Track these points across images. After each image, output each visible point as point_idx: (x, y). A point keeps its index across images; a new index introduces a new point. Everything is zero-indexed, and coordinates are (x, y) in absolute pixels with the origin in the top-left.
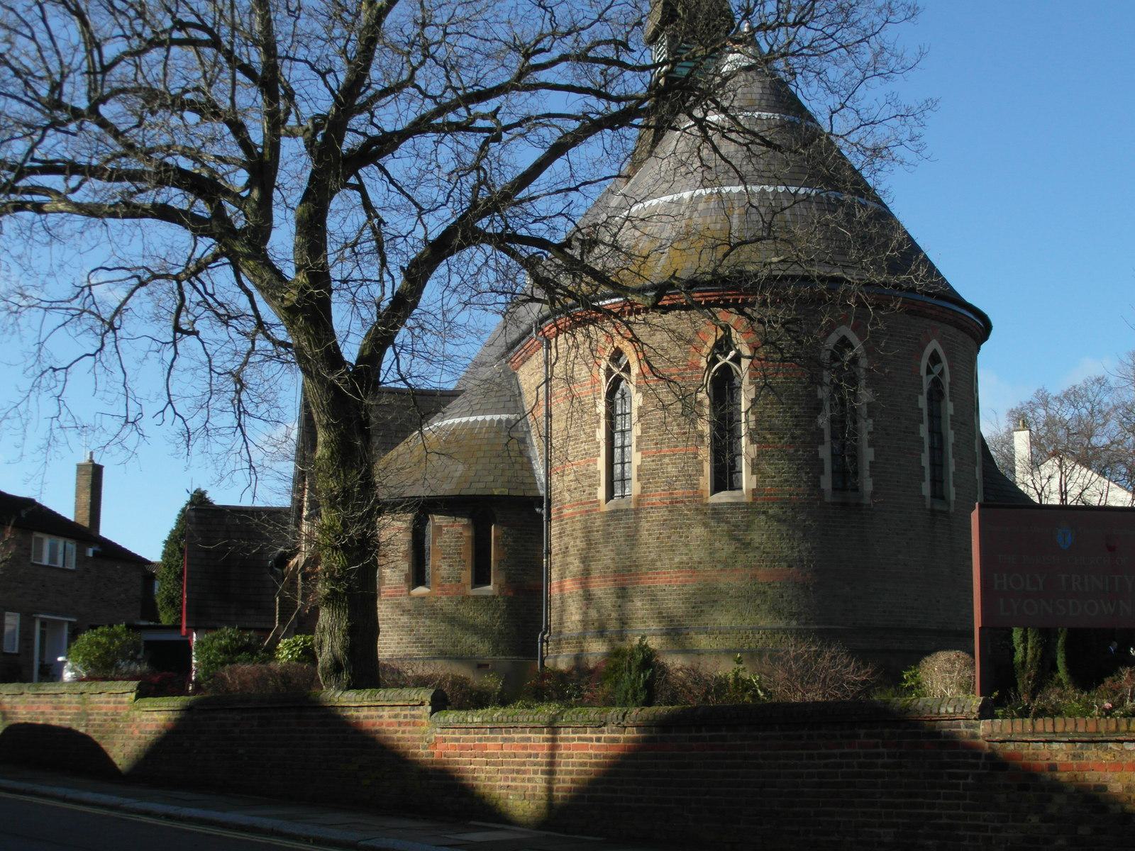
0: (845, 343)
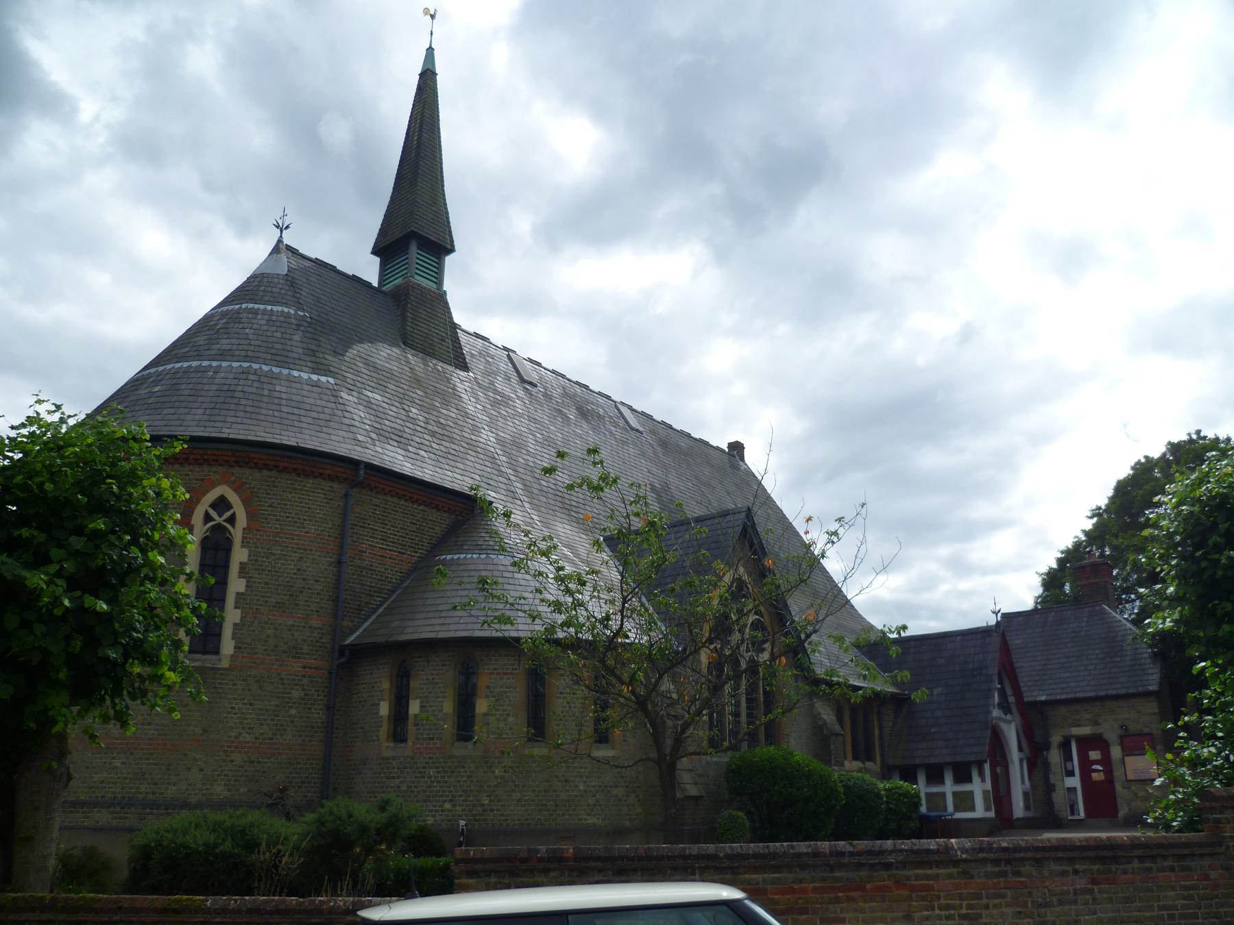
0: (221, 504)
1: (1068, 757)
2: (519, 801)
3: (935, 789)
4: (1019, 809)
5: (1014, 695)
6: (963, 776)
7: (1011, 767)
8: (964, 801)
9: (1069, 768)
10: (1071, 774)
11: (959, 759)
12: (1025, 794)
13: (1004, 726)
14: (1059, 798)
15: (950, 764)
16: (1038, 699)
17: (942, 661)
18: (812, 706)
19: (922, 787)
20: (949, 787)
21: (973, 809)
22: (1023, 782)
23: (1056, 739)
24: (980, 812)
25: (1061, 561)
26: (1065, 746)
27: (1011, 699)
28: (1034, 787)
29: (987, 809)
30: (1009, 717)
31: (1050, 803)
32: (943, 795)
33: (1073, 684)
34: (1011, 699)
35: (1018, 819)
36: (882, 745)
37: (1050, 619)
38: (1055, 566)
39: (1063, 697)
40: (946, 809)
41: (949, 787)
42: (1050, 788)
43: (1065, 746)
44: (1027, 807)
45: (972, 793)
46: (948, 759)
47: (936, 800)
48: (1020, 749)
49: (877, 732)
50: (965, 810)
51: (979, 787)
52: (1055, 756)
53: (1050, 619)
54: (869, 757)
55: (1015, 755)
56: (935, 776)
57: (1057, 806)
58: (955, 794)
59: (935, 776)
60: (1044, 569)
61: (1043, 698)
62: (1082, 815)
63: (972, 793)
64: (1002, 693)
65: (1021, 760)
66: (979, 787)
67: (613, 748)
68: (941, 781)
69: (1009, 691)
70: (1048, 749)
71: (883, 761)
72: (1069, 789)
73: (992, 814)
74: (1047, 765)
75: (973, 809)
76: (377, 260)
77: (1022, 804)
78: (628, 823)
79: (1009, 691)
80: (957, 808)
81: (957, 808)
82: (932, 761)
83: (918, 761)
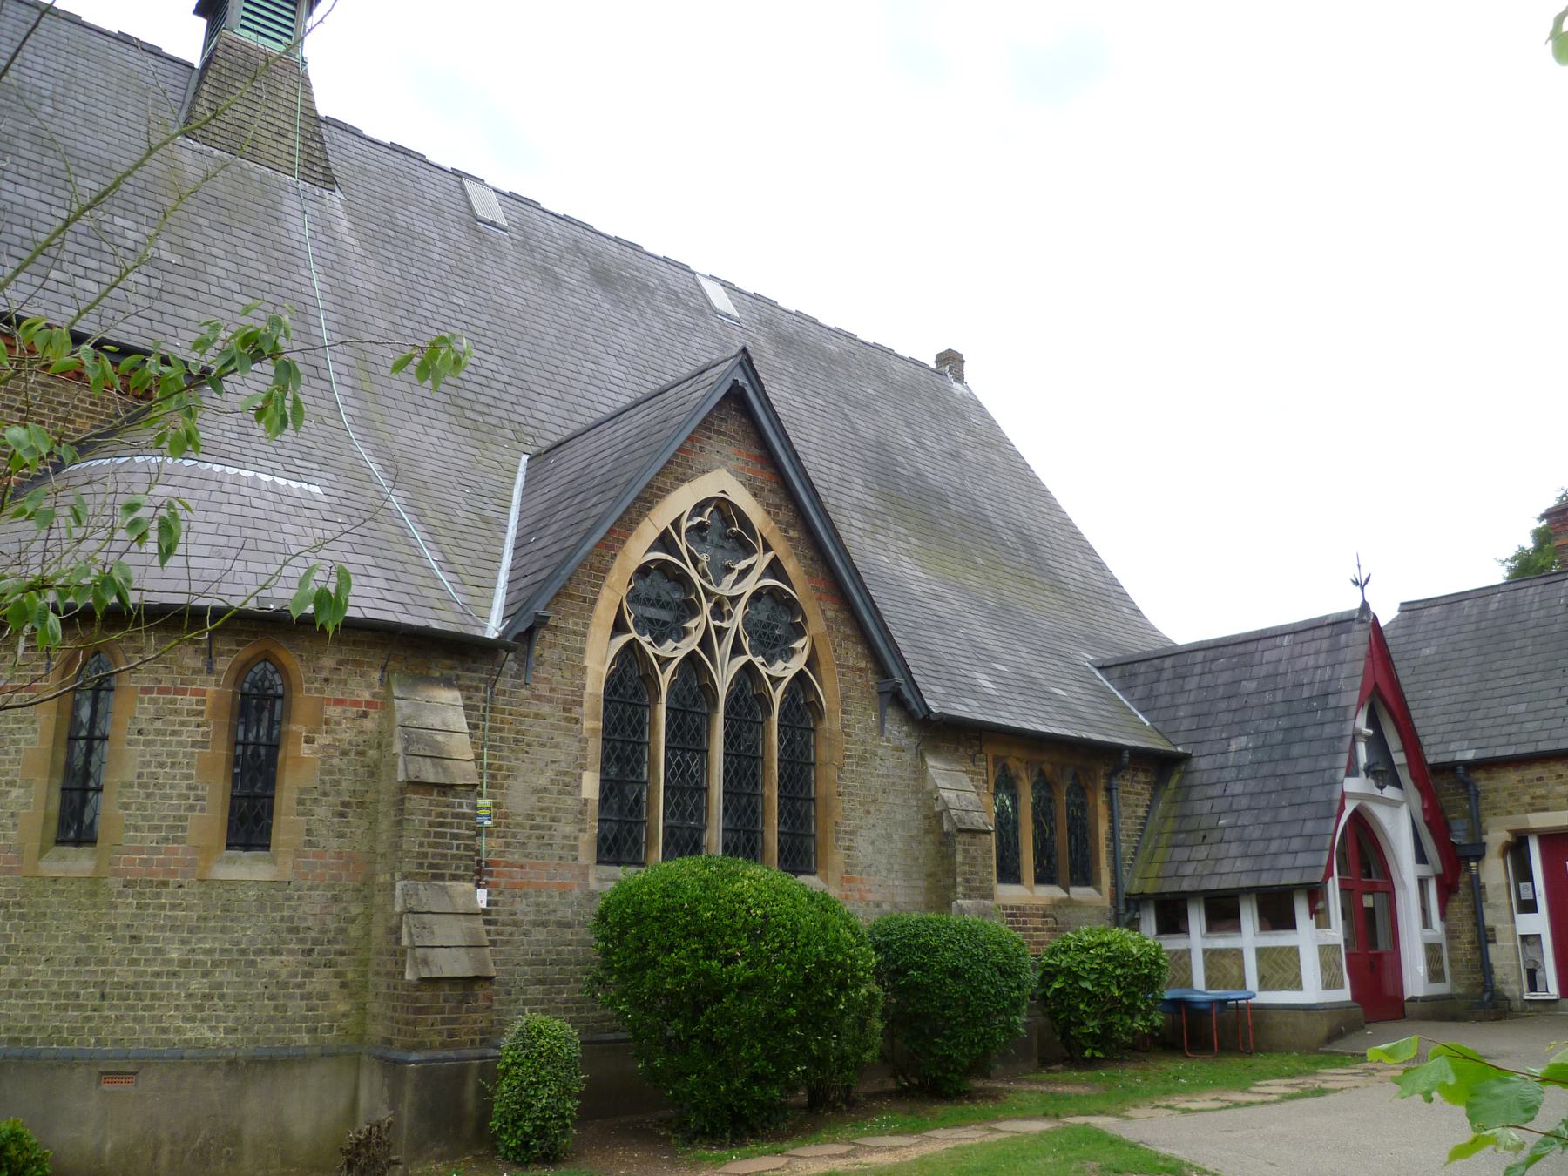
1: (1524, 874)
2: (13, 984)
3: (1221, 942)
4: (1415, 980)
5: (1406, 749)
6: (1277, 913)
7: (1400, 895)
8: (1279, 967)
9: (1526, 895)
10: (1529, 907)
11: (1267, 880)
12: (1432, 950)
13: (1381, 814)
14: (1503, 957)
15: (1248, 891)
16: (1459, 757)
17: (1252, 686)
18: (920, 772)
19: (1197, 938)
20: (1250, 937)
21: (1297, 984)
22: (1426, 923)
23: (1497, 836)
24: (1312, 990)
25: (1541, 537)
26: (1516, 848)
27: (1399, 758)
28: (1451, 934)
29: (1330, 983)
30: (1390, 792)
31: (1485, 967)
32: (1238, 954)
33: (1530, 726)
34: (1399, 758)
35: (1413, 999)
36: (1114, 854)
37: (1493, 606)
38: (1529, 544)
39: (1511, 751)
40: (1243, 986)
41: (1250, 937)
42: (1484, 937)
43: (1516, 848)
44: (1435, 975)
45: (1294, 951)
46: (1246, 882)
47: (1222, 965)
48: (1421, 857)
49: (1103, 827)
50: (1282, 987)
51: (1314, 940)
52: (1494, 872)
53: (1493, 606)
54: (1083, 874)
55: (1407, 869)
56: (1222, 912)
57: (1499, 974)
58: (1261, 953)
59: (1222, 912)
60: (1512, 551)
61: (1470, 755)
62: (1554, 991)
63: (1294, 951)
64: (1378, 743)
65: (1422, 882)
66: (1314, 940)
67: (273, 861)
68: (1289, 923)
69: (1394, 742)
70: (1479, 857)
71: (1116, 884)
72: (1524, 938)
73: (1344, 994)
74: (1477, 889)
75: (1297, 984)
76: (202, 23)
77: (1422, 969)
78: (305, 1039)
79: (1394, 742)
80: (1264, 984)
81: (1264, 984)
82: (1213, 884)
83: (1186, 886)
